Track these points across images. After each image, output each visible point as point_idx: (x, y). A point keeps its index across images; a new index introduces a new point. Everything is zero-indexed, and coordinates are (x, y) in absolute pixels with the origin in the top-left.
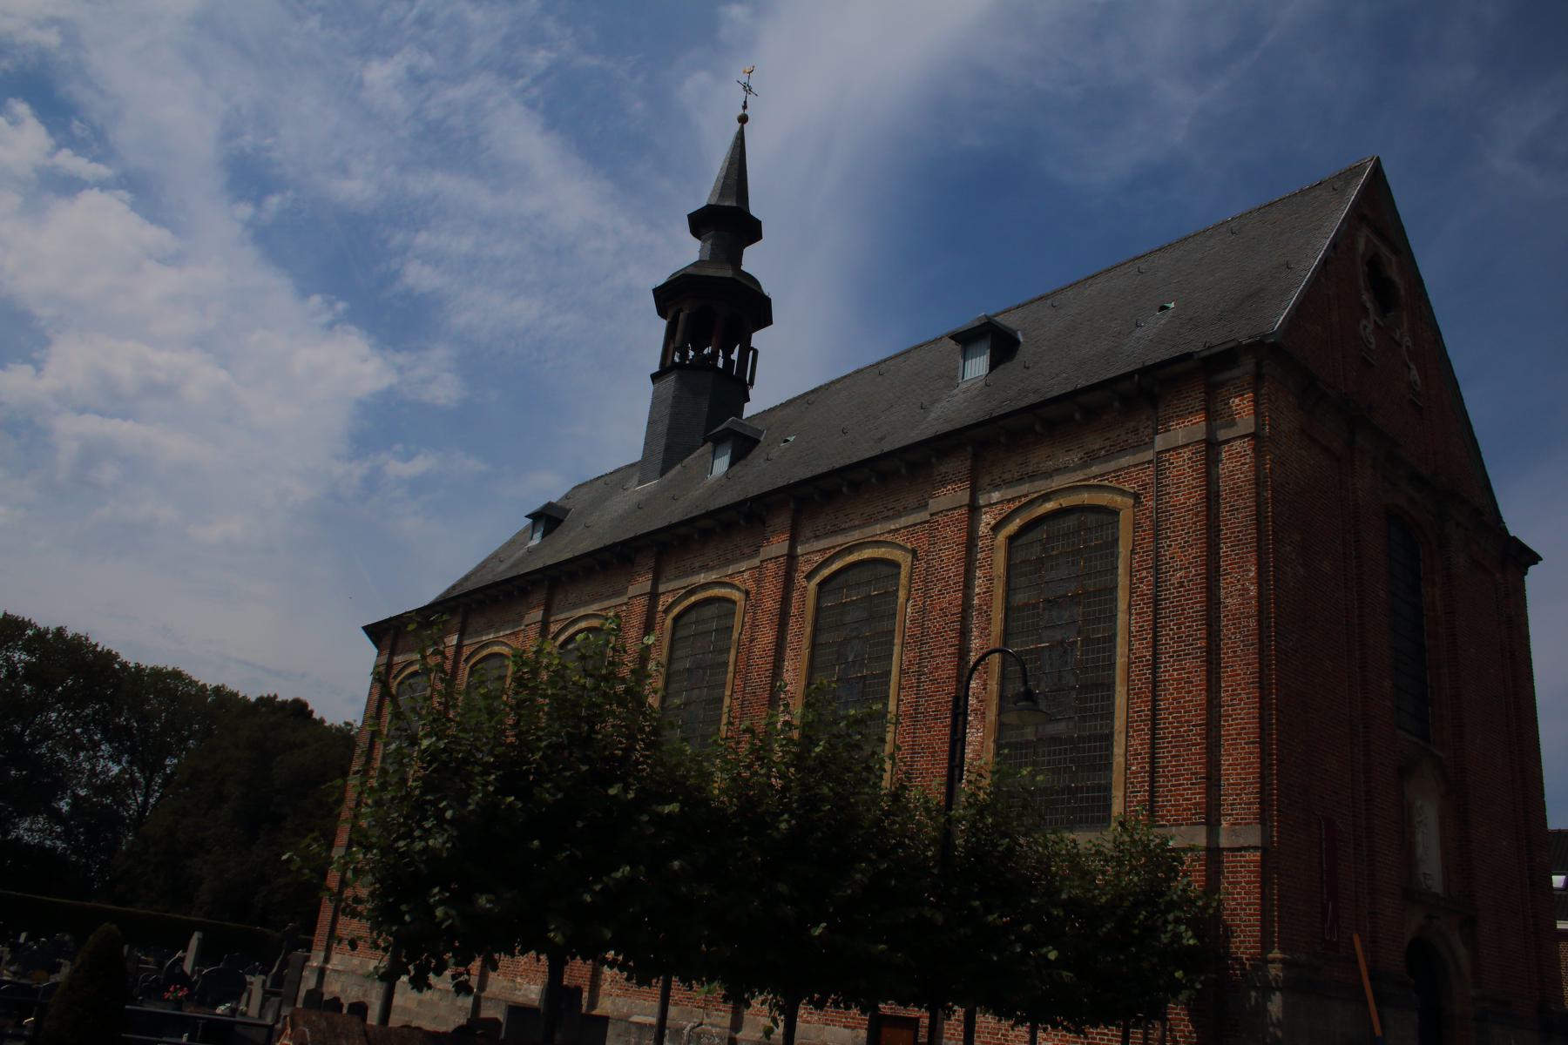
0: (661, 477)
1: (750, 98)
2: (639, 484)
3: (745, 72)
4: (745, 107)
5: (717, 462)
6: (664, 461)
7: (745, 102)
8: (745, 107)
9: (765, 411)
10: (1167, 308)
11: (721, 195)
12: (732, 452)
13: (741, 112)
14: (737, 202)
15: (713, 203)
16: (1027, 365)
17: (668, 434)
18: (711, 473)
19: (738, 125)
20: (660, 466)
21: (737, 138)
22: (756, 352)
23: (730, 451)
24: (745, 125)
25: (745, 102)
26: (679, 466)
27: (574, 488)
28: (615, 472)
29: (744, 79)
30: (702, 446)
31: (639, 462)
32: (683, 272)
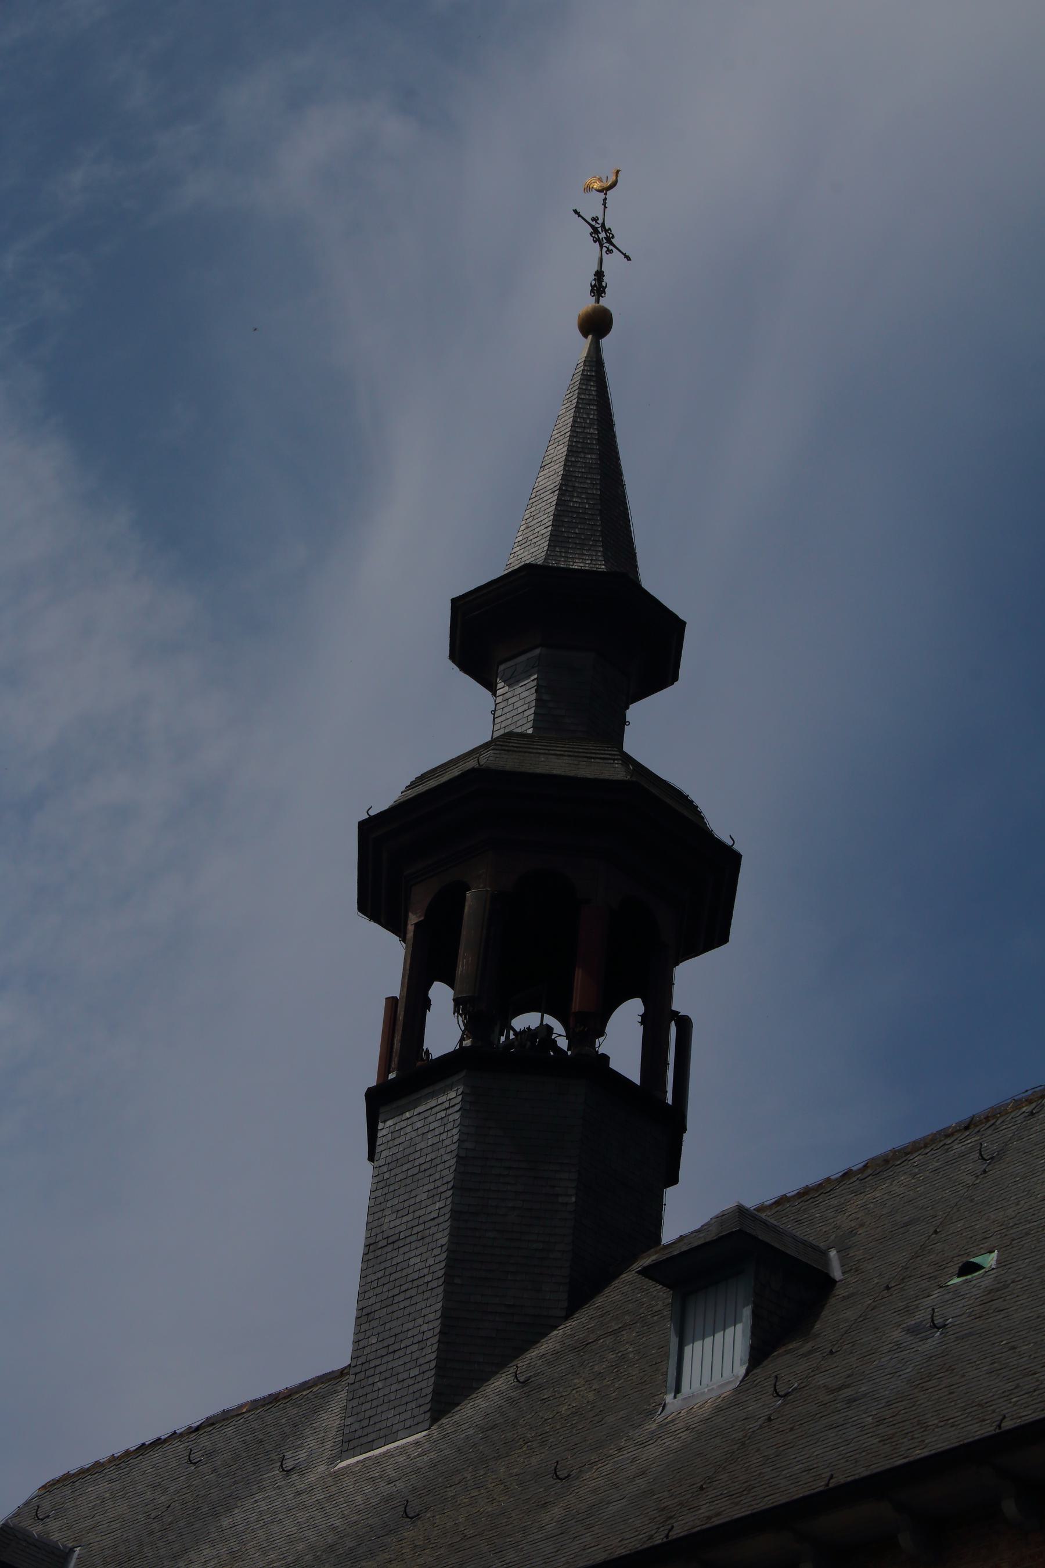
0: (434, 1420)
1: (613, 263)
2: (349, 1444)
3: (588, 189)
4: (598, 289)
5: (694, 1352)
6: (442, 1367)
7: (599, 275)
8: (598, 289)
9: (828, 1180)
10: (978, 1267)
11: (556, 539)
12: (755, 1315)
13: (588, 303)
14: (606, 560)
15: (540, 562)
16: (938, 1321)
17: (449, 1277)
18: (678, 1390)
19: (583, 345)
20: (427, 1385)
21: (585, 379)
22: (685, 1025)
23: (747, 1312)
24: (605, 342)
25: (599, 275)
26: (501, 1383)
27: (49, 1488)
28: (211, 1423)
29: (592, 207)
30: (567, 1317)
31: (342, 1373)
32: (471, 764)
